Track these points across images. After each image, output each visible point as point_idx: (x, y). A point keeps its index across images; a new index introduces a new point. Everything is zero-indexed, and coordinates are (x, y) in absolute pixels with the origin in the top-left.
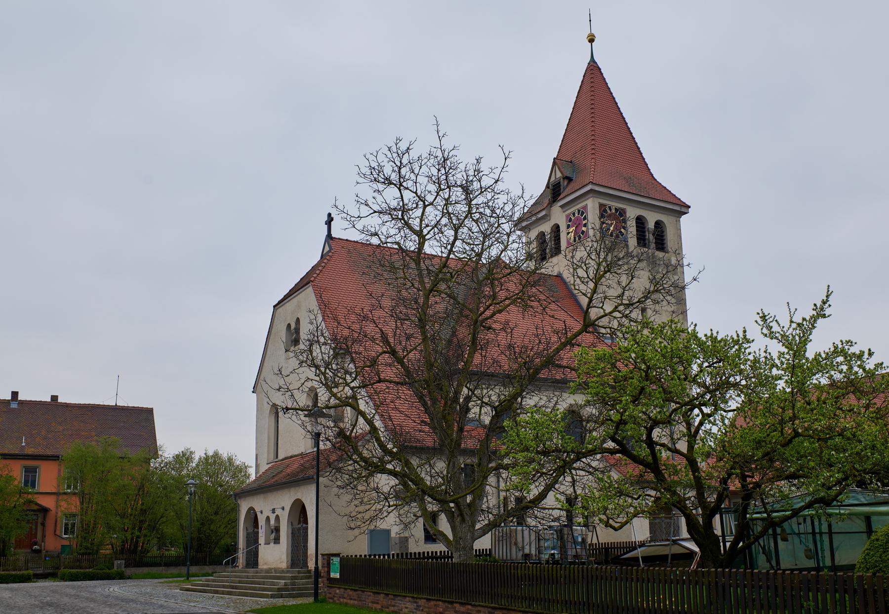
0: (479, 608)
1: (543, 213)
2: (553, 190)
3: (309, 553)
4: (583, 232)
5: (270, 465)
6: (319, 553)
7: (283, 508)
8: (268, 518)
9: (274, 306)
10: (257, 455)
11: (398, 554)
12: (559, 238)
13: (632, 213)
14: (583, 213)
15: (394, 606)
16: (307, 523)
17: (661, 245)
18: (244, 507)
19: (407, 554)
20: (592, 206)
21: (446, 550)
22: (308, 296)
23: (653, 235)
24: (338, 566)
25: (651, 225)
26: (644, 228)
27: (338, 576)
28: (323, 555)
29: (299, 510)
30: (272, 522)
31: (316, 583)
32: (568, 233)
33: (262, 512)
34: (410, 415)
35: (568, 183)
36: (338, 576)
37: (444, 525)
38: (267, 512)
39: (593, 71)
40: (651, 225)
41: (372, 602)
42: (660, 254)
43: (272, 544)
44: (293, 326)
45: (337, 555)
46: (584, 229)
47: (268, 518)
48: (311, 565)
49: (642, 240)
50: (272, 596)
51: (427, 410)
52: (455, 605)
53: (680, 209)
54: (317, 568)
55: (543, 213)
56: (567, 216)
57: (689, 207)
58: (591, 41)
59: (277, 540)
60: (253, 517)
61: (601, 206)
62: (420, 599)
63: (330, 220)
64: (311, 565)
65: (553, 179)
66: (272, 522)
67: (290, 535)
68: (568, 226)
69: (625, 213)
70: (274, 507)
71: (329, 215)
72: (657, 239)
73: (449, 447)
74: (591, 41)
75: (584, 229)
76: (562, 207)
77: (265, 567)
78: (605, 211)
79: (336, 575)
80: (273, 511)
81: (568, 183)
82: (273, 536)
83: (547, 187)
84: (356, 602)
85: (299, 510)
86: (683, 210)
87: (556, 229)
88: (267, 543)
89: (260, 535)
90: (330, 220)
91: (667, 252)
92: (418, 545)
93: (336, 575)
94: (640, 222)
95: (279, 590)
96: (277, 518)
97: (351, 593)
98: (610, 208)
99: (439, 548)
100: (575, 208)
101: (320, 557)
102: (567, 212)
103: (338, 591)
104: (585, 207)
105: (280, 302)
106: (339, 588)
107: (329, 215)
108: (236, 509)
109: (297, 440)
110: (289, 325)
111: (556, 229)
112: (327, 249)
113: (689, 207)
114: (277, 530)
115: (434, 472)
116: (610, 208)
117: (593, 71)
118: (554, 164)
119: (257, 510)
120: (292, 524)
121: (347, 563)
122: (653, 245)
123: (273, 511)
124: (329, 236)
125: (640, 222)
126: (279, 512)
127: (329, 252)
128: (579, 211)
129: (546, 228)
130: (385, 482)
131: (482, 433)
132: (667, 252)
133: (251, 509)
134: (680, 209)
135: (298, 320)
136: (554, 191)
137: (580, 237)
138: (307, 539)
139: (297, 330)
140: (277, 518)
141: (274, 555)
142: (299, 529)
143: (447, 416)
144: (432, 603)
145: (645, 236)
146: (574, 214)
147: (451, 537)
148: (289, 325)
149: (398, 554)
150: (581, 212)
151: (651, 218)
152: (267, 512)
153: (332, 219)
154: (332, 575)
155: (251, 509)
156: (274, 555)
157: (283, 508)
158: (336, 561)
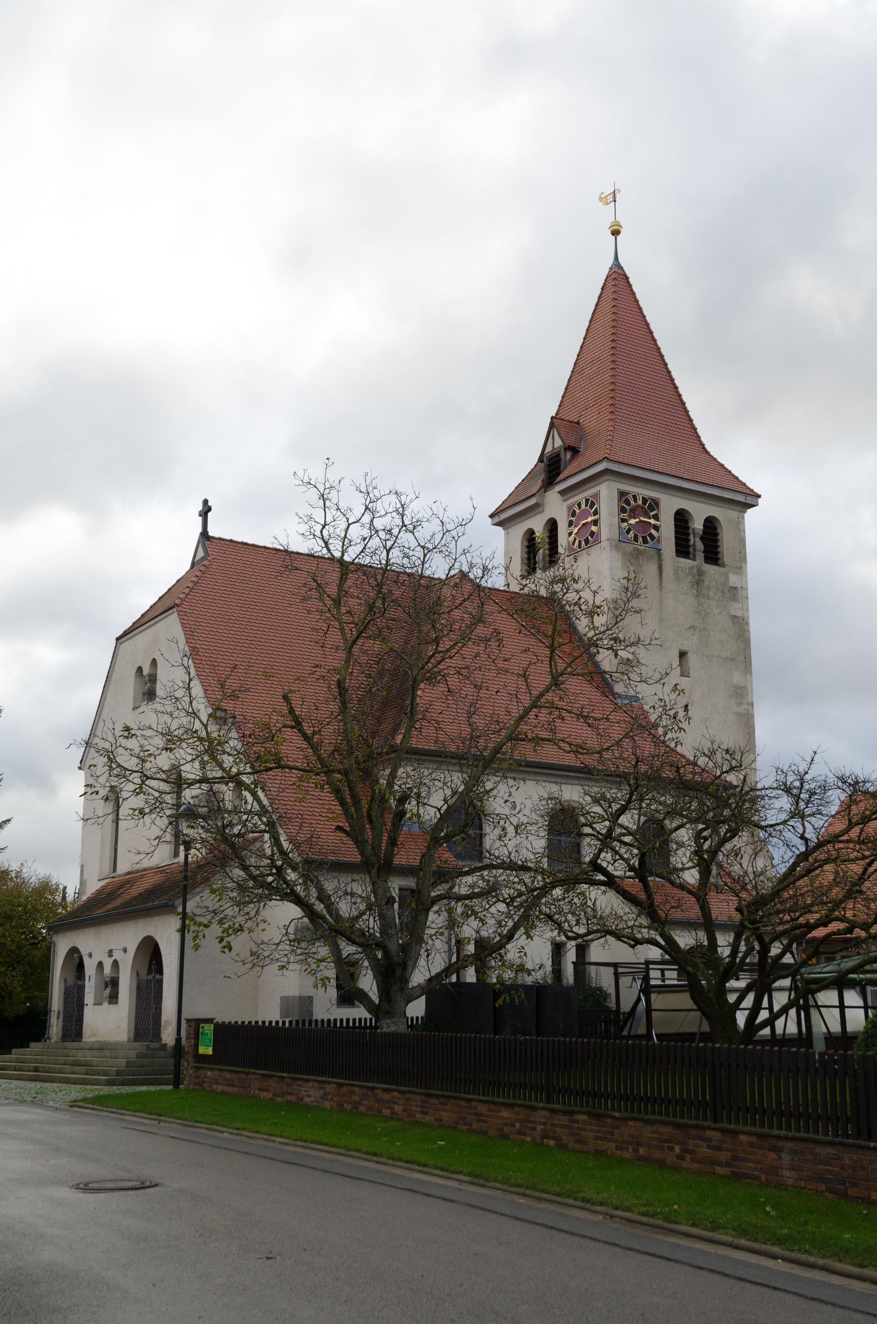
0: (408, 1096)
1: (533, 501)
2: (549, 466)
3: (164, 1017)
4: (592, 534)
5: (103, 883)
6: (183, 1016)
7: (125, 950)
8: (100, 965)
9: (117, 639)
10: (82, 867)
11: (297, 1022)
12: (557, 535)
13: (669, 504)
14: (593, 504)
15: (291, 1094)
16: (161, 973)
17: (713, 555)
18: (62, 946)
19: (310, 1021)
20: (607, 493)
21: (369, 1016)
22: (172, 625)
23: (702, 538)
24: (211, 1035)
25: (698, 525)
26: (688, 528)
27: (210, 1051)
28: (188, 1021)
29: (151, 952)
30: (107, 970)
31: (178, 1065)
32: (570, 534)
33: (90, 955)
34: (319, 818)
35: (572, 458)
36: (210, 1051)
37: (368, 982)
38: (100, 955)
39: (618, 282)
40: (698, 525)
41: (260, 1089)
42: (711, 569)
43: (106, 1005)
44: (146, 672)
45: (209, 1021)
46: (594, 528)
47: (100, 965)
48: (168, 1036)
49: (683, 549)
50: (109, 1083)
51: (346, 811)
52: (376, 1091)
53: (747, 499)
54: (178, 1040)
55: (533, 501)
56: (570, 508)
57: (759, 496)
58: (616, 233)
59: (113, 998)
60: (77, 961)
61: (622, 494)
62: (329, 1083)
63: (206, 510)
64: (168, 1036)
65: (549, 448)
66: (107, 970)
67: (135, 990)
68: (571, 524)
69: (657, 505)
70: (109, 948)
71: (206, 502)
72: (707, 545)
73: (377, 866)
74: (616, 233)
75: (594, 528)
76: (562, 493)
77: (93, 1039)
78: (627, 502)
79: (206, 1050)
80: (110, 953)
81: (572, 458)
82: (108, 991)
83: (541, 460)
84: (236, 1090)
85: (151, 952)
86: (750, 500)
87: (552, 526)
88: (98, 1003)
89: (87, 990)
90: (206, 510)
91: (723, 565)
92: (327, 1008)
93: (206, 1050)
94: (682, 519)
95: (118, 1073)
96: (116, 964)
97: (228, 1075)
98: (635, 497)
99: (359, 1013)
100: (580, 497)
101: (183, 1022)
102: (569, 502)
103: (209, 1074)
104: (597, 496)
105: (126, 633)
106: (212, 1069)
107: (206, 502)
108: (48, 952)
109: (147, 846)
110: (140, 670)
111: (552, 526)
112: (201, 554)
113: (759, 496)
114: (114, 983)
115: (350, 897)
116: (635, 497)
117: (618, 282)
118: (552, 426)
119: (84, 952)
120: (65, 982)
121: (227, 1034)
122: (700, 556)
123: (110, 953)
124: (205, 535)
125: (682, 519)
126: (117, 955)
127: (203, 559)
128: (587, 500)
129: (538, 524)
130: (283, 914)
131: (423, 844)
132: (723, 565)
133: (74, 951)
134: (747, 499)
135: (154, 662)
136: (551, 468)
137: (587, 541)
138: (161, 998)
139: (153, 678)
140: (116, 964)
141: (108, 1022)
142: (149, 982)
143: (372, 822)
144: (345, 1089)
145: (689, 540)
146: (579, 505)
147: (375, 998)
148: (140, 670)
149: (297, 1022)
150: (591, 503)
151: (699, 513)
152: (100, 955)
153: (210, 509)
154: (202, 1050)
155: (74, 951)
156: (108, 1022)
157: (125, 950)
158: (209, 1029)
